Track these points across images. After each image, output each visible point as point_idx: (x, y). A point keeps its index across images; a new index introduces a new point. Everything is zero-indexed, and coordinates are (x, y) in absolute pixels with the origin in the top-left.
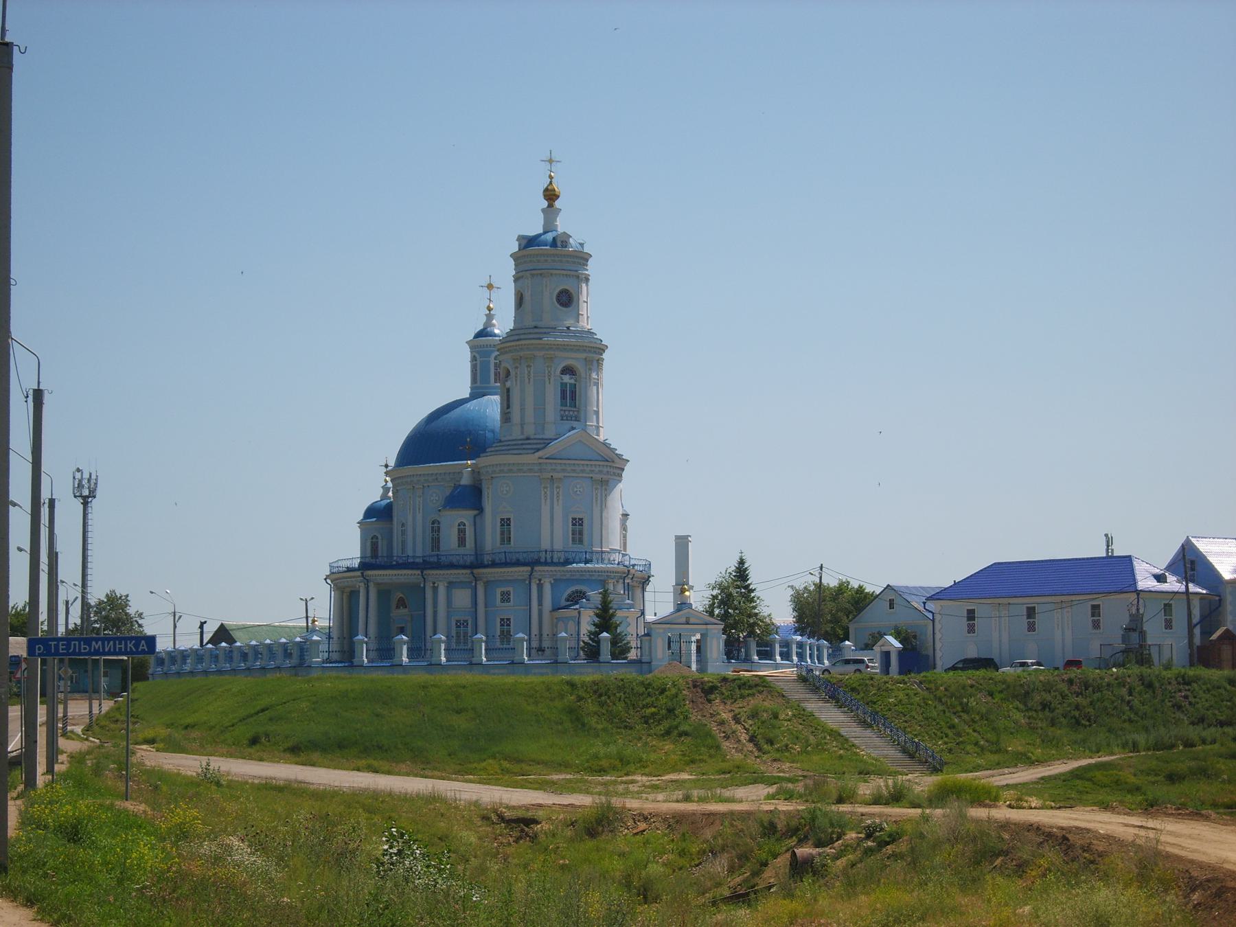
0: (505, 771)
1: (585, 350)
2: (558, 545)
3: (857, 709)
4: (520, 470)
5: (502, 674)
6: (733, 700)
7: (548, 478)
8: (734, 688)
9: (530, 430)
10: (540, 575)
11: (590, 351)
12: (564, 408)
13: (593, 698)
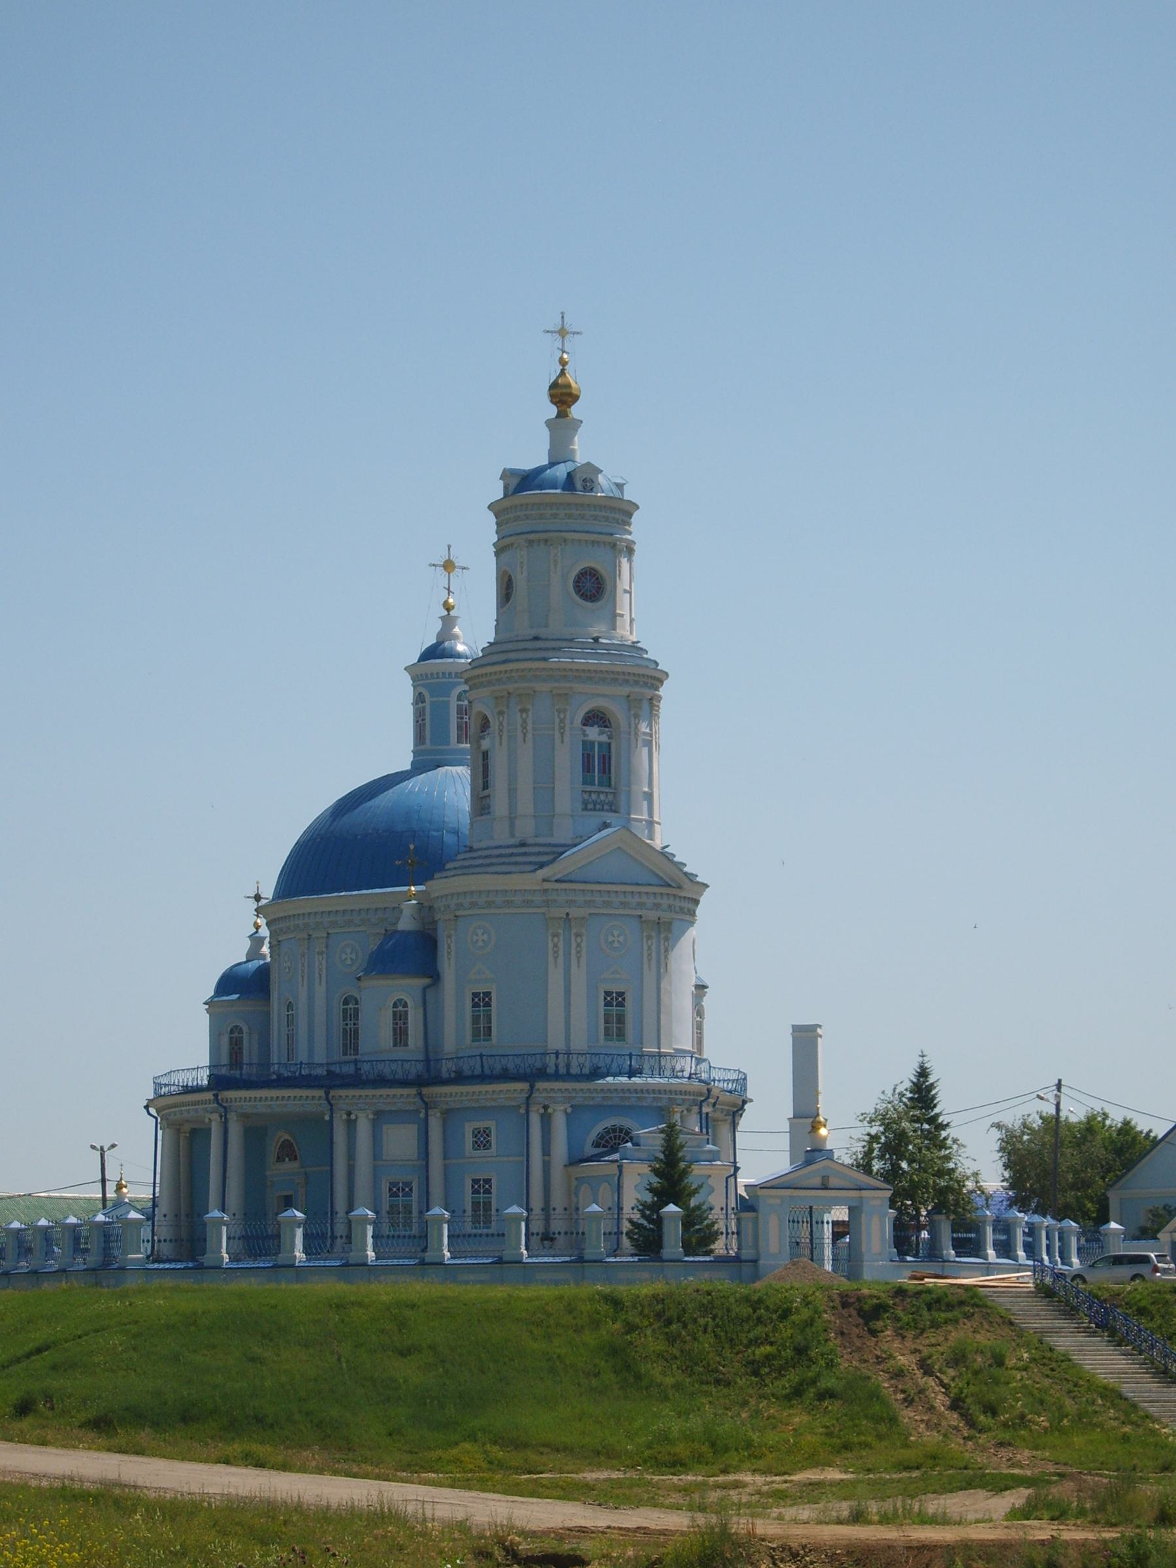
0: (495, 1465)
1: (627, 681)
2: (579, 1042)
3: (1152, 1347)
4: (509, 904)
5: (482, 1282)
6: (918, 1331)
7: (561, 918)
8: (919, 1308)
9: (526, 828)
10: (546, 1098)
11: (636, 683)
12: (589, 788)
13: (655, 1326)
